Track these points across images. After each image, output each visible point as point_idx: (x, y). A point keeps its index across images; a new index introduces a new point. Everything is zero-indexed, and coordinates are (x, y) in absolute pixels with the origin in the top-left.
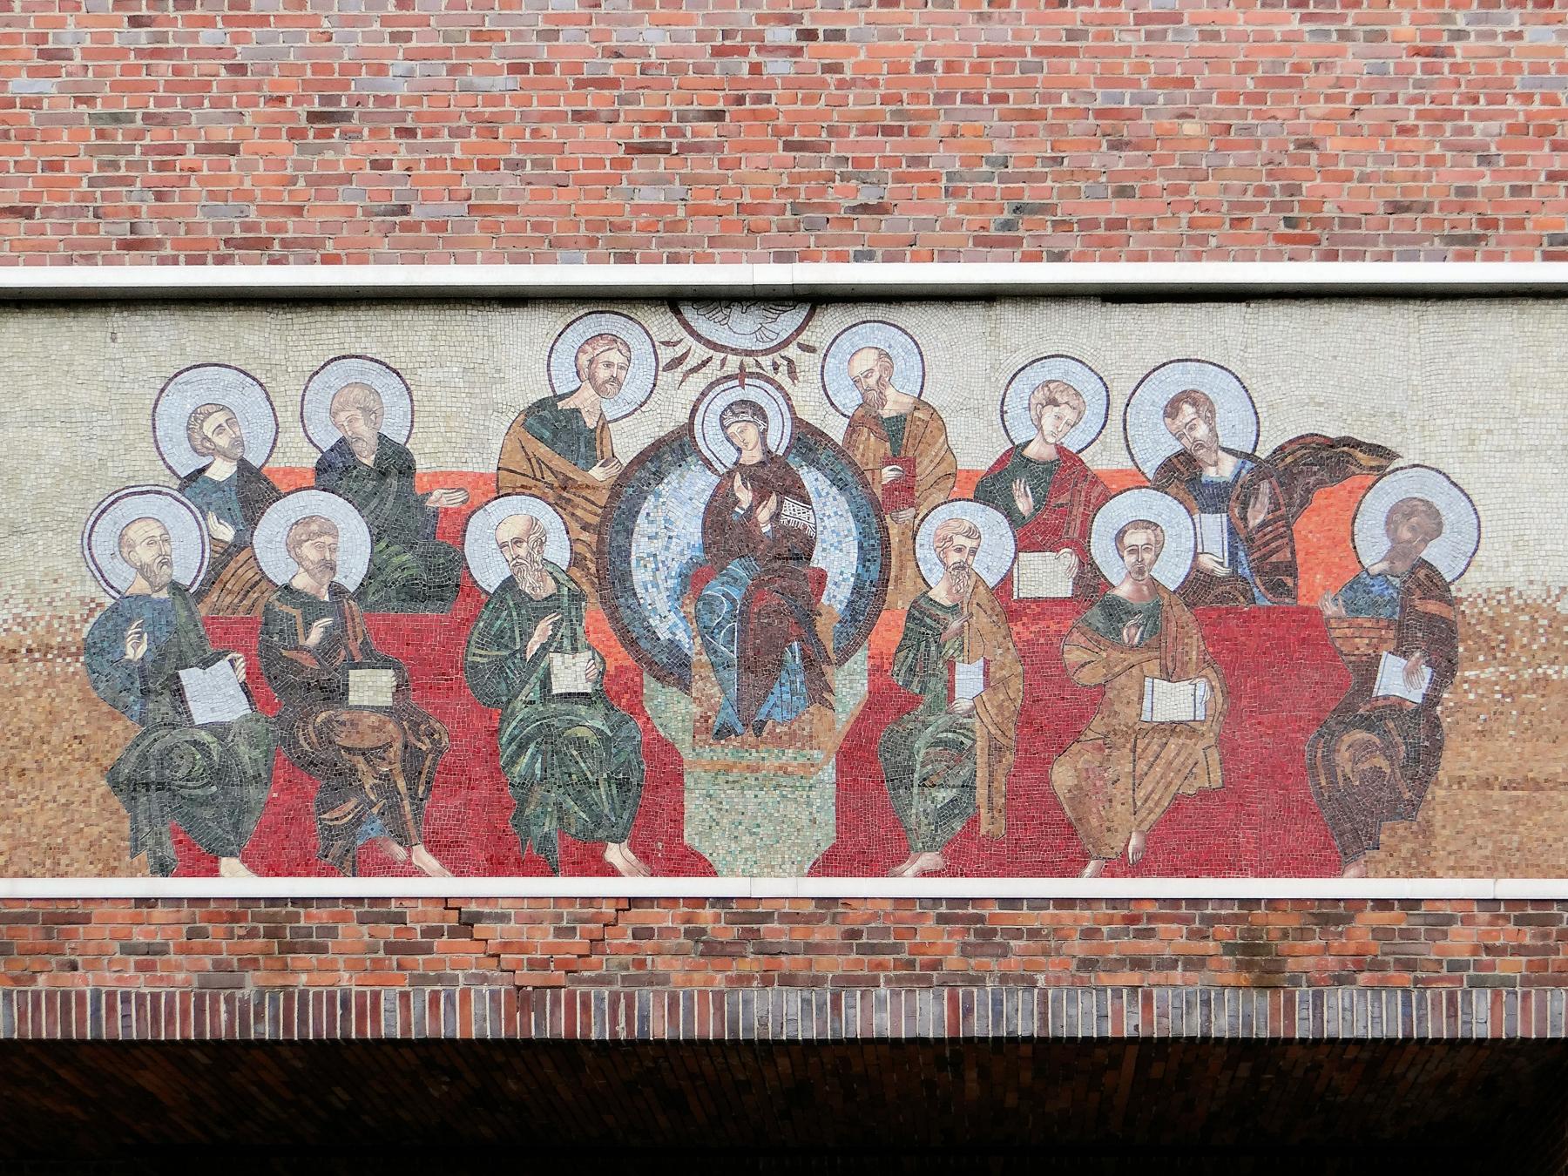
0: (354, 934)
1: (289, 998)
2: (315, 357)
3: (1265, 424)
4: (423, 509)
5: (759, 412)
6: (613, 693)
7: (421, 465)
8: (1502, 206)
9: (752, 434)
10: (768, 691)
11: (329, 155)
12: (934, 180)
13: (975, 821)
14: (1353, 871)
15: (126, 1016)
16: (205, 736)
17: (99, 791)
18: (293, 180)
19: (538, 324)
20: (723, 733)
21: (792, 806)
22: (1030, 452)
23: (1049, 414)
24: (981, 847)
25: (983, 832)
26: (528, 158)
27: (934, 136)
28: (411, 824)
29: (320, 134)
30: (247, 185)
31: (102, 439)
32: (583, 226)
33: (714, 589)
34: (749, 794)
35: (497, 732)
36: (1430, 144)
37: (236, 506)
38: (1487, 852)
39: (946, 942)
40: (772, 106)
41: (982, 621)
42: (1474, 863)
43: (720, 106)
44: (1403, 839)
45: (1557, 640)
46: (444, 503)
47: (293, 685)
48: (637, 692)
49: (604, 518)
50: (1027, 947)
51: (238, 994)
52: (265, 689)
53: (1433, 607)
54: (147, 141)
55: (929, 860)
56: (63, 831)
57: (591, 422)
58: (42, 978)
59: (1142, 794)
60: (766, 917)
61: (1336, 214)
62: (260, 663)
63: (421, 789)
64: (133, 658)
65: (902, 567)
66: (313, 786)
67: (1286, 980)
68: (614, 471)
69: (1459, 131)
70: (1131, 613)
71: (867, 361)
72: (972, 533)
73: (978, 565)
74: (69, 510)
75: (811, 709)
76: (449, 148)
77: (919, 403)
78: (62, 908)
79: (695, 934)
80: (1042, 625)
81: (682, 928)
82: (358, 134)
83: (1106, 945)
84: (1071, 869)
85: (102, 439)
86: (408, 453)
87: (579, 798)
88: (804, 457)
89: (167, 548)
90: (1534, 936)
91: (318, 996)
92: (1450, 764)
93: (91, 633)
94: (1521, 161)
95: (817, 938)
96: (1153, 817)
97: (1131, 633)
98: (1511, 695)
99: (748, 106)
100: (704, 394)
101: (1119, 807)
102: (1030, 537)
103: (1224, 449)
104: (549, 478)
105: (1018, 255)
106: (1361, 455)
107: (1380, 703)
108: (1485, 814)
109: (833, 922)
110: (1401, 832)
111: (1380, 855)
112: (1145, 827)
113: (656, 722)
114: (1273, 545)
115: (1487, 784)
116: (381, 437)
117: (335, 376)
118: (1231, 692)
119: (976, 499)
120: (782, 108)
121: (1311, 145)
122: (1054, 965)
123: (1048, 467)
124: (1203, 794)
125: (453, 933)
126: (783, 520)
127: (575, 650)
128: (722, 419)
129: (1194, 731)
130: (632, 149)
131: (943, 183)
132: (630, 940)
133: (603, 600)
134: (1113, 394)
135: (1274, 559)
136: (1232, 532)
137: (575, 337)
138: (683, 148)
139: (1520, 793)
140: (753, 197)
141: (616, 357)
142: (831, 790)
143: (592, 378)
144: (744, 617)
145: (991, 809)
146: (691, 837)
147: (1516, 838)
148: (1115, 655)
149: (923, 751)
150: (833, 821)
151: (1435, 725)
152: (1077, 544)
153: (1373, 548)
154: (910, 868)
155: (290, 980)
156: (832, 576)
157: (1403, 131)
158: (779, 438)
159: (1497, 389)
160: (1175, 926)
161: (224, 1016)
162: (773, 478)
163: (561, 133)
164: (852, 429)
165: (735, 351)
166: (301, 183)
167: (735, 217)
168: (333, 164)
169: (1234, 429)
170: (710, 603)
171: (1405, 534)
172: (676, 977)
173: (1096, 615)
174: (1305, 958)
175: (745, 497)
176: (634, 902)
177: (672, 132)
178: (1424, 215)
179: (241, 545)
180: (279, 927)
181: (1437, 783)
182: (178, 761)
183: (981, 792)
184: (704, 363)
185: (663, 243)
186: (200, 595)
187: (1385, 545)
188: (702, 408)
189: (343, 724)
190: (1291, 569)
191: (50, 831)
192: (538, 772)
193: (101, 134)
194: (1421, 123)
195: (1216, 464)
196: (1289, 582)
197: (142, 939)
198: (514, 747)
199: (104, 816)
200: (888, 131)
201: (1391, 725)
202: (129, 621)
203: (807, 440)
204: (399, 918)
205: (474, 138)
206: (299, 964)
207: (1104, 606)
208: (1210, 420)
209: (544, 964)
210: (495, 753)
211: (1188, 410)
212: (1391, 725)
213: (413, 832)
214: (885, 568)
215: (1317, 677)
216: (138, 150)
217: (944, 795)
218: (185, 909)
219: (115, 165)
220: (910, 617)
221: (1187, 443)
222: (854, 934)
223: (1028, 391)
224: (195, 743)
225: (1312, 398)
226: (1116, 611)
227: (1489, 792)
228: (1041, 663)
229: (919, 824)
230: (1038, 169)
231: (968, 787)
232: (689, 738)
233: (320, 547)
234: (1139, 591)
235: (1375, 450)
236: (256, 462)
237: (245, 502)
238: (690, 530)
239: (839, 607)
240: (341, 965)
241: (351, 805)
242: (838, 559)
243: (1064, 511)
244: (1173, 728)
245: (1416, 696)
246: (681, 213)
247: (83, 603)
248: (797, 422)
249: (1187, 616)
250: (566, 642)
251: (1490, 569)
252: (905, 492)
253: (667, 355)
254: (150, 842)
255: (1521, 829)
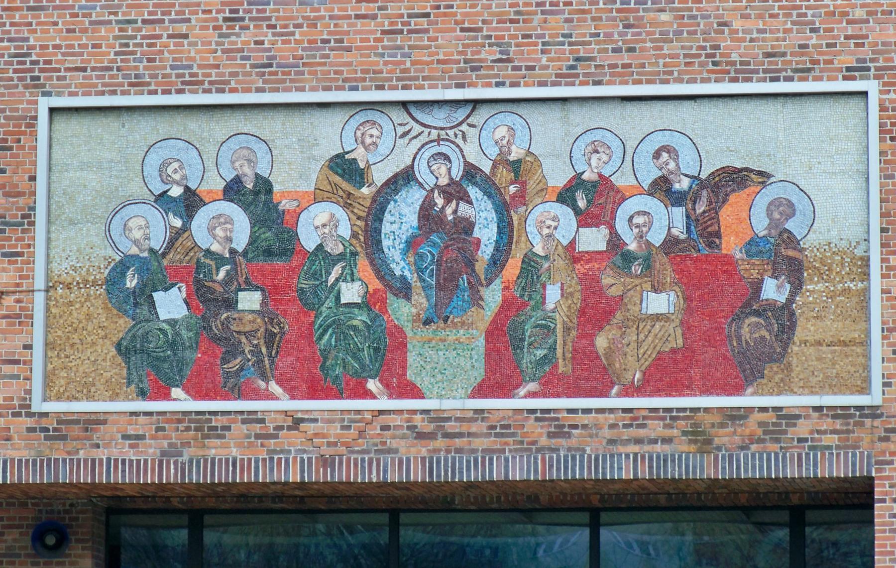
0: (240, 429)
1: (206, 461)
2: (224, 134)
3: (704, 162)
4: (277, 210)
5: (447, 158)
6: (371, 302)
7: (276, 188)
8: (821, 53)
9: (443, 170)
10: (451, 300)
11: (233, 38)
12: (535, 46)
13: (556, 366)
14: (750, 390)
15: (123, 471)
16: (166, 326)
17: (111, 354)
18: (216, 51)
19: (338, 117)
20: (427, 322)
21: (462, 359)
22: (585, 176)
23: (595, 157)
24: (559, 379)
25: (560, 371)
26: (332, 38)
27: (535, 23)
28: (268, 370)
29: (228, 28)
30: (192, 54)
31: (117, 177)
32: (359, 72)
33: (424, 249)
34: (441, 353)
35: (312, 324)
36: (785, 23)
37: (183, 209)
38: (820, 379)
39: (538, 432)
40: (454, 10)
41: (560, 263)
42: (813, 385)
43: (428, 10)
44: (776, 373)
45: (854, 269)
46: (287, 207)
47: (209, 299)
48: (383, 301)
49: (369, 214)
50: (581, 433)
51: (180, 459)
52: (195, 301)
53: (791, 253)
54: (143, 33)
55: (532, 386)
56: (93, 375)
57: (362, 165)
58: (81, 452)
59: (641, 351)
60: (448, 419)
61: (738, 59)
62: (193, 288)
63: (274, 352)
64: (130, 284)
65: (519, 236)
66: (220, 351)
67: (714, 448)
68: (374, 189)
69: (799, 15)
70: (636, 259)
71: (502, 132)
72: (555, 218)
73: (558, 235)
74: (99, 213)
75: (473, 309)
76: (293, 34)
77: (529, 153)
78: (93, 417)
79: (411, 428)
80: (590, 265)
81: (405, 425)
82: (248, 28)
83: (622, 431)
84: (604, 394)
85: (117, 177)
86: (270, 183)
87: (355, 357)
88: (470, 181)
89: (148, 231)
90: (841, 425)
91: (220, 460)
92: (800, 334)
93: (109, 274)
94: (832, 30)
95: (474, 430)
96: (647, 363)
97: (636, 269)
98: (831, 298)
99: (442, 10)
100: (419, 150)
101: (630, 358)
102: (585, 219)
103: (683, 174)
104: (341, 193)
105: (577, 82)
106: (753, 176)
107: (764, 303)
108: (818, 359)
109: (482, 421)
110: (775, 369)
111: (764, 381)
112: (643, 368)
113: (393, 317)
114: (709, 223)
115: (819, 343)
116: (257, 175)
117: (233, 144)
118: (688, 299)
119: (557, 201)
120: (459, 11)
121: (725, 24)
122: (595, 442)
123: (594, 184)
124: (674, 351)
125: (289, 428)
126: (459, 213)
127: (353, 280)
128: (428, 162)
129: (668, 318)
130: (384, 32)
131: (540, 47)
132: (379, 431)
133: (368, 255)
134: (627, 147)
135: (709, 229)
136: (688, 217)
137: (354, 123)
138: (410, 32)
139: (836, 348)
140: (444, 55)
141: (375, 132)
142: (482, 350)
143: (363, 143)
144: (439, 263)
145: (564, 360)
146: (410, 375)
147: (834, 371)
148: (628, 280)
149: (530, 330)
150: (483, 367)
151: (792, 314)
152: (609, 223)
153: (760, 224)
154: (522, 391)
155: (206, 452)
156: (484, 240)
157: (771, 16)
158: (457, 172)
159: (822, 141)
160: (656, 422)
161: (172, 471)
162: (454, 192)
163: (349, 25)
164: (494, 167)
165: (435, 128)
166: (219, 53)
167: (435, 66)
168: (236, 43)
169: (688, 163)
170: (421, 257)
171: (776, 216)
172: (402, 450)
173: (618, 259)
174: (724, 438)
175: (440, 201)
176: (381, 412)
177: (403, 24)
178: (782, 59)
179: (185, 228)
180: (204, 427)
181: (794, 343)
182: (151, 338)
183: (559, 351)
184: (420, 134)
185: (399, 79)
186: (164, 255)
187: (767, 222)
188: (418, 157)
189: (235, 319)
190: (718, 235)
191: (86, 375)
192: (333, 343)
193: (121, 30)
194: (781, 12)
195: (679, 182)
196: (717, 241)
197: (132, 433)
198: (321, 330)
199: (113, 368)
200: (512, 21)
201: (770, 314)
202: (129, 268)
203: (471, 172)
204: (262, 421)
205: (305, 29)
206: (211, 445)
207: (622, 255)
208: (676, 161)
209: (335, 444)
210: (311, 335)
211: (665, 155)
212: (770, 314)
213: (269, 374)
214: (511, 237)
215: (731, 290)
216: (139, 37)
217: (540, 353)
218: (155, 417)
219: (127, 45)
220: (523, 261)
221: (665, 172)
222: (493, 427)
223: (584, 146)
224: (160, 330)
225: (728, 148)
226: (628, 258)
227: (820, 348)
228: (591, 286)
229: (527, 367)
230: (588, 39)
231: (553, 349)
232: (410, 325)
233: (225, 230)
234: (641, 247)
235: (760, 173)
236: (193, 187)
237: (187, 207)
238: (412, 219)
239: (487, 257)
240: (232, 445)
241: (238, 361)
242: (486, 233)
243: (602, 207)
244: (657, 317)
245: (782, 299)
246: (408, 64)
247: (105, 259)
248: (467, 164)
249: (665, 259)
250: (348, 277)
251: (820, 233)
252: (521, 197)
253: (401, 130)
254: (136, 380)
255: (837, 366)
